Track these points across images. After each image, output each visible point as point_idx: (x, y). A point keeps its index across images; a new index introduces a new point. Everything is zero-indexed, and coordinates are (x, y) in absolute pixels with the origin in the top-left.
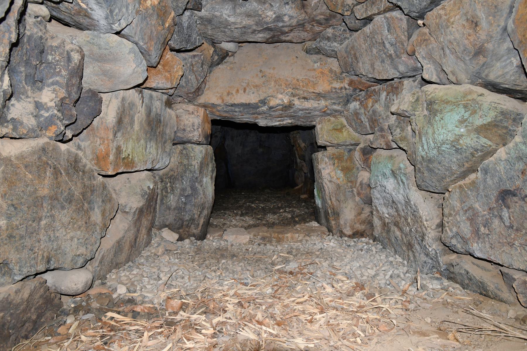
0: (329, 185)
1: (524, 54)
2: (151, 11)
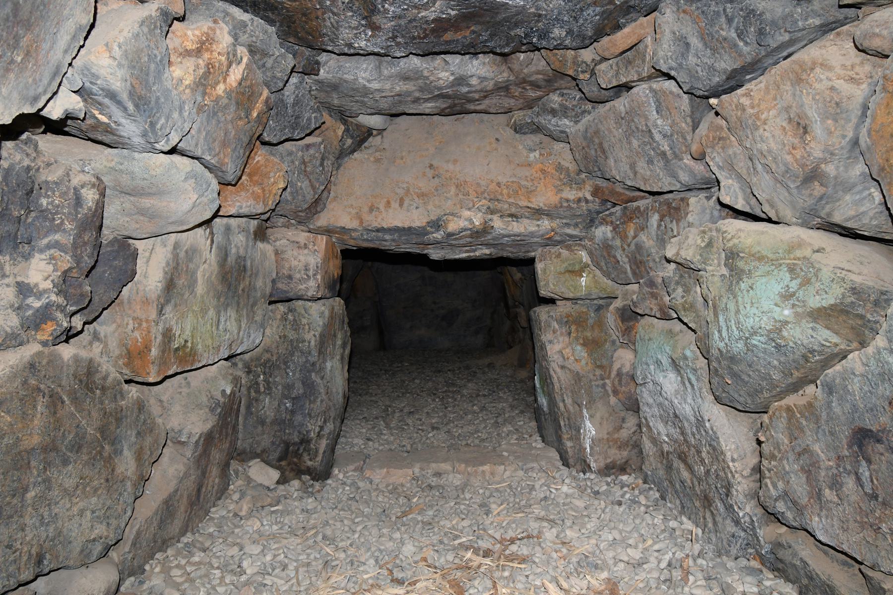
0: (560, 374)
1: (889, 190)
2: (225, 101)
